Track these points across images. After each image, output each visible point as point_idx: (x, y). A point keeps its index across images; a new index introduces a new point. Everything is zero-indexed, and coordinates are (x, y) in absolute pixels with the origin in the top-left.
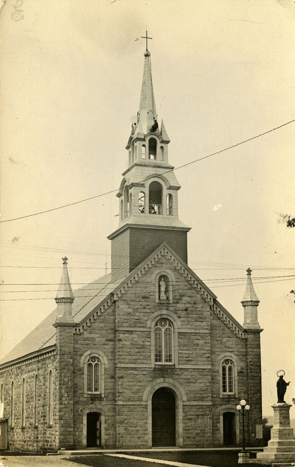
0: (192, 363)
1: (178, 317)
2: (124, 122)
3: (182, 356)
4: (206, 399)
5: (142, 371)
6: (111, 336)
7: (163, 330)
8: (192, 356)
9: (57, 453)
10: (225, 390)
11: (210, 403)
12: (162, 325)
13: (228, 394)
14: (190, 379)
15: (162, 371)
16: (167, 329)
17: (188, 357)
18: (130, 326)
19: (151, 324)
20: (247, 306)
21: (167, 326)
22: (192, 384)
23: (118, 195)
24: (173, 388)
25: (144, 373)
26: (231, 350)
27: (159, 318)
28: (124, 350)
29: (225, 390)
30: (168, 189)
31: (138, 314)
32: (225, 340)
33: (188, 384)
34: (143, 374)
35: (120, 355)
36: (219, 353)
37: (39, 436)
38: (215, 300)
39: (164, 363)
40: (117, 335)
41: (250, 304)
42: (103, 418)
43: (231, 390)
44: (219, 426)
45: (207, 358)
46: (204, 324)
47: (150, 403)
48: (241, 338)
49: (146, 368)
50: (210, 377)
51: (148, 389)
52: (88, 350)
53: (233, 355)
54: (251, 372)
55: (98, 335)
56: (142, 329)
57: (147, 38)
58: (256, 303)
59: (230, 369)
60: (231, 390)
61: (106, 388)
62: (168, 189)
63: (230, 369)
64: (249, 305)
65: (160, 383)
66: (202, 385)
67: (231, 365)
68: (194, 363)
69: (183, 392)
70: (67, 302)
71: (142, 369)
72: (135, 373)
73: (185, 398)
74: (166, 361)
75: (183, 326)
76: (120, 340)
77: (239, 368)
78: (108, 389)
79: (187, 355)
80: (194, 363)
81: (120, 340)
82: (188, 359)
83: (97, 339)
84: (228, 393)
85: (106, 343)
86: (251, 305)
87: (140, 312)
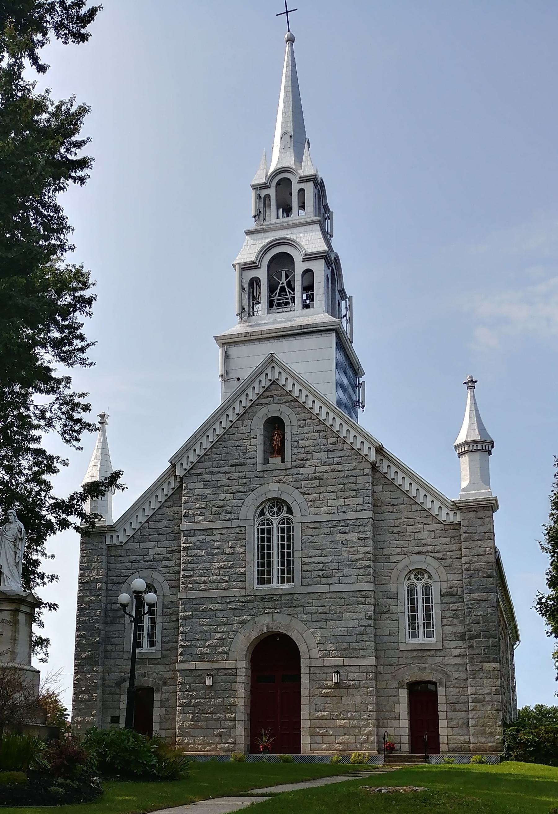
0: (331, 580)
3: (309, 568)
4: (362, 653)
5: (228, 603)
7: (275, 522)
8: (332, 566)
12: (277, 513)
13: (421, 642)
17: (322, 570)
22: (330, 623)
23: (242, 265)
24: (285, 632)
26: (425, 549)
28: (307, 610)
30: (305, 260)
31: (222, 496)
34: (230, 609)
35: (187, 577)
36: (398, 558)
41: (479, 447)
45: (364, 568)
46: (360, 500)
49: (234, 596)
50: (371, 607)
53: (429, 559)
54: (471, 591)
55: (153, 544)
57: (287, 12)
59: (427, 590)
61: (166, 639)
62: (305, 260)
63: (427, 590)
64: (475, 451)
65: (265, 623)
66: (354, 623)
67: (429, 580)
69: (313, 642)
74: (282, 581)
75: (312, 510)
78: (168, 642)
79: (320, 566)
80: (336, 580)
82: (321, 573)
83: (151, 552)
85: (168, 555)
86: (479, 450)
87: (226, 493)
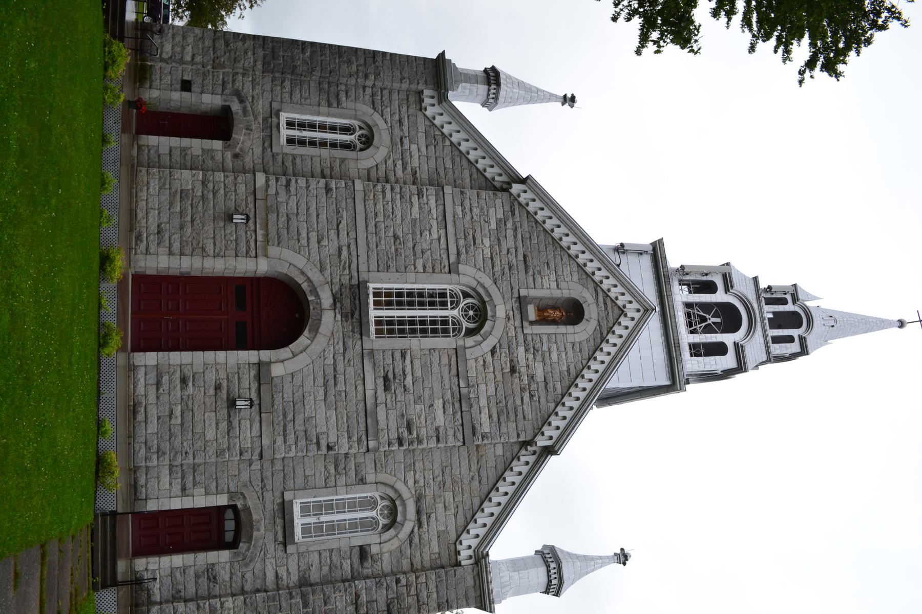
1: (494, 347)
2: (823, 294)
6: (423, 175)
10: (290, 124)
14: (335, 385)
15: (352, 303)
16: (460, 323)
19: (470, 275)
20: (549, 571)
21: (465, 324)
25: (345, 252)
27: (486, 299)
29: (290, 124)
30: (736, 345)
32: (449, 496)
33: (321, 381)
36: (411, 482)
37: (213, 459)
38: (550, 451)
40: (432, 190)
42: (217, 144)
43: (306, 530)
44: (196, 492)
47: (262, 267)
48: (459, 547)
51: (300, 261)
52: (386, 122)
70: (488, 95)
71: (353, 247)
72: (341, 226)
76: (420, 194)
81: (420, 194)
83: (414, 147)
84: (285, 132)
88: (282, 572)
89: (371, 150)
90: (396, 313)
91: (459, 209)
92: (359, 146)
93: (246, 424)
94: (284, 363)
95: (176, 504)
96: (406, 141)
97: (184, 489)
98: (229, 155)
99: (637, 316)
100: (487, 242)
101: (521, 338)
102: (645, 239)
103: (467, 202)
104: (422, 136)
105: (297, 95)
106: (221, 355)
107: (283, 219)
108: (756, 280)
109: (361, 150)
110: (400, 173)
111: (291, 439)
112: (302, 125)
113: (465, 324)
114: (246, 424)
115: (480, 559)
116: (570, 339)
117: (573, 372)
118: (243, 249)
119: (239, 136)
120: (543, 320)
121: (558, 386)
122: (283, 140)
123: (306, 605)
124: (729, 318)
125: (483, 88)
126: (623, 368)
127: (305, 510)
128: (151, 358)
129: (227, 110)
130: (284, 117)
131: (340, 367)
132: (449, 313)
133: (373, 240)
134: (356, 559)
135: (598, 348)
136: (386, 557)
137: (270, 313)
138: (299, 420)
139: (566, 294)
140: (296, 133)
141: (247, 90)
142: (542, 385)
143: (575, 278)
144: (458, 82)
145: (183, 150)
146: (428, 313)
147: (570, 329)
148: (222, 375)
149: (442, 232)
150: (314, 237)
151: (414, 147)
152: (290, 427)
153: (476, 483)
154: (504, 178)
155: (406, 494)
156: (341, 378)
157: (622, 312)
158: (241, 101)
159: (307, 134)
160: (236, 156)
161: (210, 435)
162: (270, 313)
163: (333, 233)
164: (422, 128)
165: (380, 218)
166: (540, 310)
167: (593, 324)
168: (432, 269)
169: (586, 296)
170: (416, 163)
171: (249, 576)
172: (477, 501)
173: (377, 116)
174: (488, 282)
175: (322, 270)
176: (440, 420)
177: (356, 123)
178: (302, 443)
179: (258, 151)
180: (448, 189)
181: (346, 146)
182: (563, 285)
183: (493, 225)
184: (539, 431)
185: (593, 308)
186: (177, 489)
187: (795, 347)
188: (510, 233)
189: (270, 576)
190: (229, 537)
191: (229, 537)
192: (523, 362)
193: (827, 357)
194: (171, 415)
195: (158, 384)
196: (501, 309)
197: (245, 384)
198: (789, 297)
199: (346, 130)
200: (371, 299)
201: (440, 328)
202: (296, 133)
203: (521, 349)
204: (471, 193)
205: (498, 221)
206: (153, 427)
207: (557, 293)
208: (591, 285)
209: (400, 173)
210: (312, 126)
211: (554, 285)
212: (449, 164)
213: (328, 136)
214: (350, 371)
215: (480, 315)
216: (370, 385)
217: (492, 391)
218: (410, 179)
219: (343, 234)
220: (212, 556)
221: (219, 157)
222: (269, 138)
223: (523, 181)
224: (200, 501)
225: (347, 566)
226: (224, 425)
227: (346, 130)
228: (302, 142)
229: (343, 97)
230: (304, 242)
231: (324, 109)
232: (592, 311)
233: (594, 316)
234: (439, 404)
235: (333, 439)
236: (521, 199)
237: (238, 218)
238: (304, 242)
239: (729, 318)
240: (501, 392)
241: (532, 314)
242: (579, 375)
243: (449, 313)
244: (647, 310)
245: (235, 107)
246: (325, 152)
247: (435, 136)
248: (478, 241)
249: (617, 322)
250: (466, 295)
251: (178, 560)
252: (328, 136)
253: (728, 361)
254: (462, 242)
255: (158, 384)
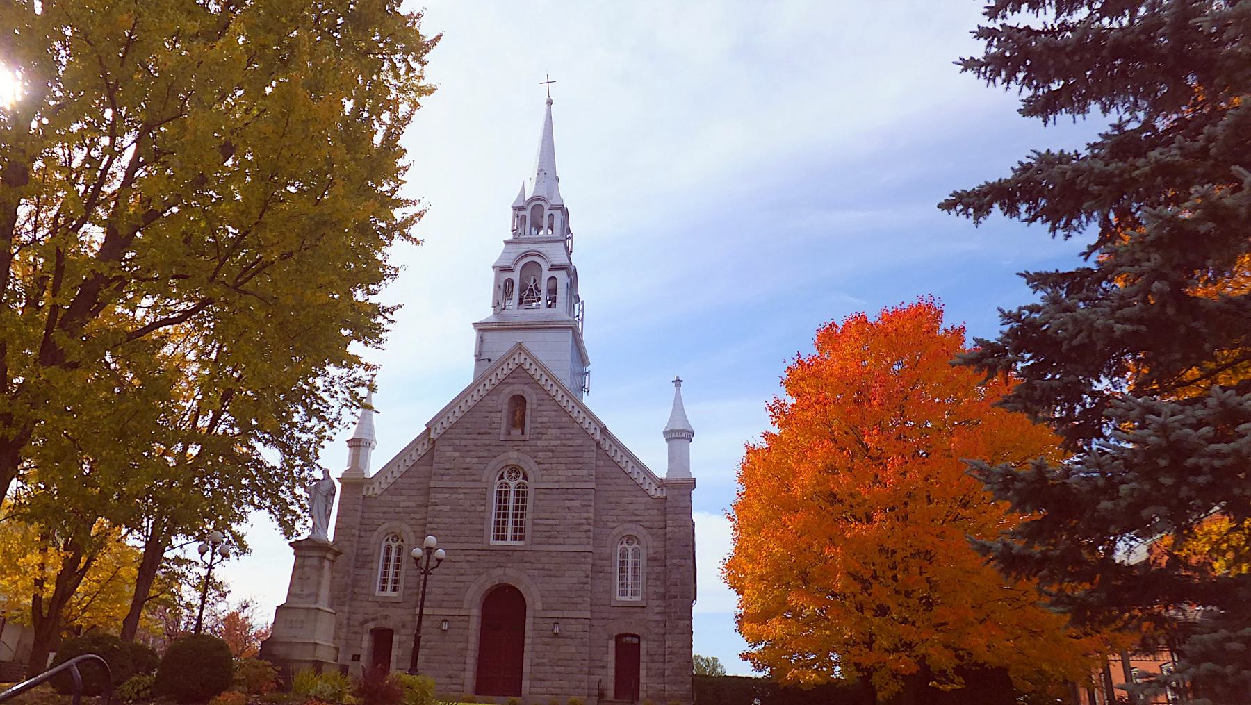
0: (557, 541)
2: (522, 180)
9: (60, 326)
11: (588, 615)
18: (451, 480)
21: (520, 480)
25: (470, 558)
29: (383, 589)
30: (550, 270)
38: (604, 430)
39: (509, 542)
40: (432, 495)
42: (396, 638)
46: (585, 472)
47: (476, 612)
51: (474, 587)
56: (471, 485)
58: (688, 435)
60: (519, 534)
62: (550, 270)
65: (498, 576)
68: (561, 541)
73: (539, 606)
77: (651, 551)
88: (658, 610)
89: (404, 535)
90: (510, 526)
91: (445, 478)
92: (400, 542)
93: (569, 627)
94: (535, 604)
95: (612, 672)
96: (397, 510)
97: (603, 667)
98: (403, 631)
99: (523, 356)
100: (468, 460)
101: (532, 443)
102: (473, 334)
103: (442, 472)
104: (395, 498)
105: (362, 584)
106: (527, 641)
107: (447, 598)
108: (507, 243)
109: (525, 478)
110: (419, 516)
111: (580, 600)
112: (384, 581)
113: (520, 480)
114: (569, 627)
115: (662, 483)
116: (535, 407)
117: (556, 408)
118: (464, 624)
119: (389, 624)
120: (522, 425)
121: (564, 419)
122: (394, 594)
123: (675, 597)
124: (531, 268)
125: (362, 450)
126: (558, 375)
127: (624, 593)
128: (525, 684)
129: (372, 631)
130: (379, 593)
131: (540, 566)
132: (512, 490)
133: (462, 539)
134: (655, 563)
135: (542, 387)
136: (656, 544)
137: (504, 609)
138: (568, 594)
139: (505, 407)
140: (389, 585)
141: (360, 617)
142: (563, 431)
143: (495, 398)
144: (359, 470)
145: (398, 661)
146: (511, 505)
147: (528, 406)
148: (538, 640)
149: (460, 491)
150: (459, 578)
151: (402, 504)
152: (573, 600)
153: (619, 481)
154: (426, 441)
155: (620, 528)
156: (547, 566)
157: (520, 366)
158: (366, 621)
159: (390, 577)
160: (404, 626)
161: (574, 650)
162: (504, 609)
163: (458, 565)
164: (389, 498)
165: (448, 532)
166: (514, 426)
167: (526, 388)
168: (484, 499)
169: (508, 391)
170: (413, 504)
171: (656, 630)
172: (630, 482)
173: (380, 529)
174: (494, 461)
175: (479, 574)
176: (577, 503)
177: (384, 544)
178: (582, 593)
179: (400, 611)
180: (432, 484)
181: (399, 551)
182: (499, 408)
183: (457, 454)
184: (591, 437)
185: (517, 387)
186: (603, 671)
187: (557, 214)
188: (463, 443)
189: (658, 617)
190: (635, 641)
191: (635, 641)
192: (547, 443)
193: (568, 194)
194: (559, 673)
195: (541, 680)
196: (513, 457)
197: (545, 627)
198: (522, 213)
199: (388, 551)
200: (500, 543)
201: (521, 495)
202: (389, 585)
203: (539, 443)
204: (435, 468)
205: (455, 450)
206: (565, 684)
207: (505, 412)
208: (501, 387)
209: (419, 516)
210: (385, 574)
211: (499, 415)
212: (415, 480)
213: (392, 563)
214: (544, 559)
215: (515, 470)
216: (552, 548)
217: (563, 467)
218: (423, 509)
219: (457, 558)
220: (643, 652)
221: (404, 638)
222: (395, 603)
223: (428, 429)
224: (611, 658)
225: (658, 569)
226: (568, 641)
227: (388, 551)
228: (396, 581)
229: (365, 552)
230: (461, 585)
231: (374, 566)
232: (518, 389)
233: (521, 387)
234: (568, 503)
235: (582, 574)
236: (441, 432)
237: (445, 627)
238: (461, 585)
239: (531, 268)
240: (563, 460)
241: (516, 432)
242: (558, 403)
243: (512, 490)
244: (520, 347)
245: (371, 625)
246: (404, 566)
247: (394, 489)
248: (465, 466)
249: (526, 371)
250: (501, 477)
251: (643, 673)
252: (392, 563)
253: (562, 277)
254: (468, 478)
255: (541, 680)
